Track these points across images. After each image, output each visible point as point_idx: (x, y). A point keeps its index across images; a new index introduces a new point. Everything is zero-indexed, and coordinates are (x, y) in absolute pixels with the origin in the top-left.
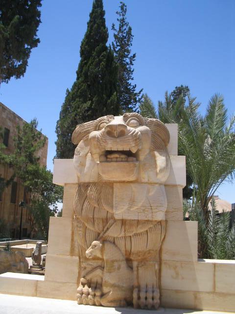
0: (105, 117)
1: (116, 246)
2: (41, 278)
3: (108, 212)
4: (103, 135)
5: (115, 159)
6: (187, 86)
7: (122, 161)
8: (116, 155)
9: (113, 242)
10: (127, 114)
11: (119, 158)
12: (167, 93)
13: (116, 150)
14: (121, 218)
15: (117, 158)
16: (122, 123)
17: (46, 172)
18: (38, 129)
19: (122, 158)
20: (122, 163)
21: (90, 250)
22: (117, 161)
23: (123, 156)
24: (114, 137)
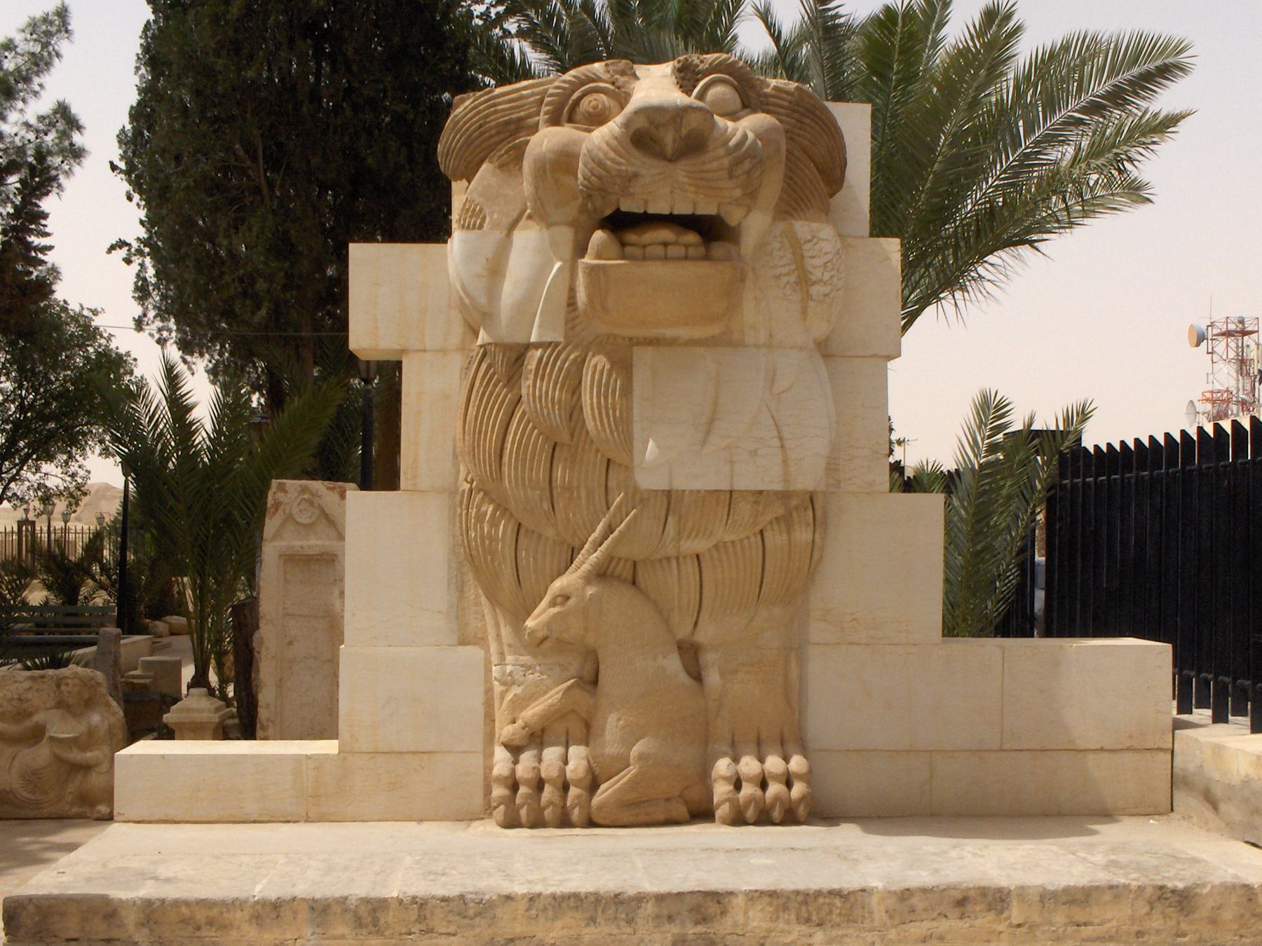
0: (598, 67)
1: (645, 594)
2: (327, 747)
3: (609, 460)
4: (617, 144)
5: (659, 250)
6: (71, 177)
7: (686, 258)
8: (665, 234)
9: (630, 577)
10: (695, 58)
11: (675, 243)
12: (114, 167)
13: (666, 212)
14: (663, 485)
15: (665, 244)
16: (678, 98)
17: (51, 288)
18: (121, 152)
19: (687, 246)
20: (688, 264)
21: (544, 617)
22: (666, 258)
23: (692, 238)
24: (661, 155)
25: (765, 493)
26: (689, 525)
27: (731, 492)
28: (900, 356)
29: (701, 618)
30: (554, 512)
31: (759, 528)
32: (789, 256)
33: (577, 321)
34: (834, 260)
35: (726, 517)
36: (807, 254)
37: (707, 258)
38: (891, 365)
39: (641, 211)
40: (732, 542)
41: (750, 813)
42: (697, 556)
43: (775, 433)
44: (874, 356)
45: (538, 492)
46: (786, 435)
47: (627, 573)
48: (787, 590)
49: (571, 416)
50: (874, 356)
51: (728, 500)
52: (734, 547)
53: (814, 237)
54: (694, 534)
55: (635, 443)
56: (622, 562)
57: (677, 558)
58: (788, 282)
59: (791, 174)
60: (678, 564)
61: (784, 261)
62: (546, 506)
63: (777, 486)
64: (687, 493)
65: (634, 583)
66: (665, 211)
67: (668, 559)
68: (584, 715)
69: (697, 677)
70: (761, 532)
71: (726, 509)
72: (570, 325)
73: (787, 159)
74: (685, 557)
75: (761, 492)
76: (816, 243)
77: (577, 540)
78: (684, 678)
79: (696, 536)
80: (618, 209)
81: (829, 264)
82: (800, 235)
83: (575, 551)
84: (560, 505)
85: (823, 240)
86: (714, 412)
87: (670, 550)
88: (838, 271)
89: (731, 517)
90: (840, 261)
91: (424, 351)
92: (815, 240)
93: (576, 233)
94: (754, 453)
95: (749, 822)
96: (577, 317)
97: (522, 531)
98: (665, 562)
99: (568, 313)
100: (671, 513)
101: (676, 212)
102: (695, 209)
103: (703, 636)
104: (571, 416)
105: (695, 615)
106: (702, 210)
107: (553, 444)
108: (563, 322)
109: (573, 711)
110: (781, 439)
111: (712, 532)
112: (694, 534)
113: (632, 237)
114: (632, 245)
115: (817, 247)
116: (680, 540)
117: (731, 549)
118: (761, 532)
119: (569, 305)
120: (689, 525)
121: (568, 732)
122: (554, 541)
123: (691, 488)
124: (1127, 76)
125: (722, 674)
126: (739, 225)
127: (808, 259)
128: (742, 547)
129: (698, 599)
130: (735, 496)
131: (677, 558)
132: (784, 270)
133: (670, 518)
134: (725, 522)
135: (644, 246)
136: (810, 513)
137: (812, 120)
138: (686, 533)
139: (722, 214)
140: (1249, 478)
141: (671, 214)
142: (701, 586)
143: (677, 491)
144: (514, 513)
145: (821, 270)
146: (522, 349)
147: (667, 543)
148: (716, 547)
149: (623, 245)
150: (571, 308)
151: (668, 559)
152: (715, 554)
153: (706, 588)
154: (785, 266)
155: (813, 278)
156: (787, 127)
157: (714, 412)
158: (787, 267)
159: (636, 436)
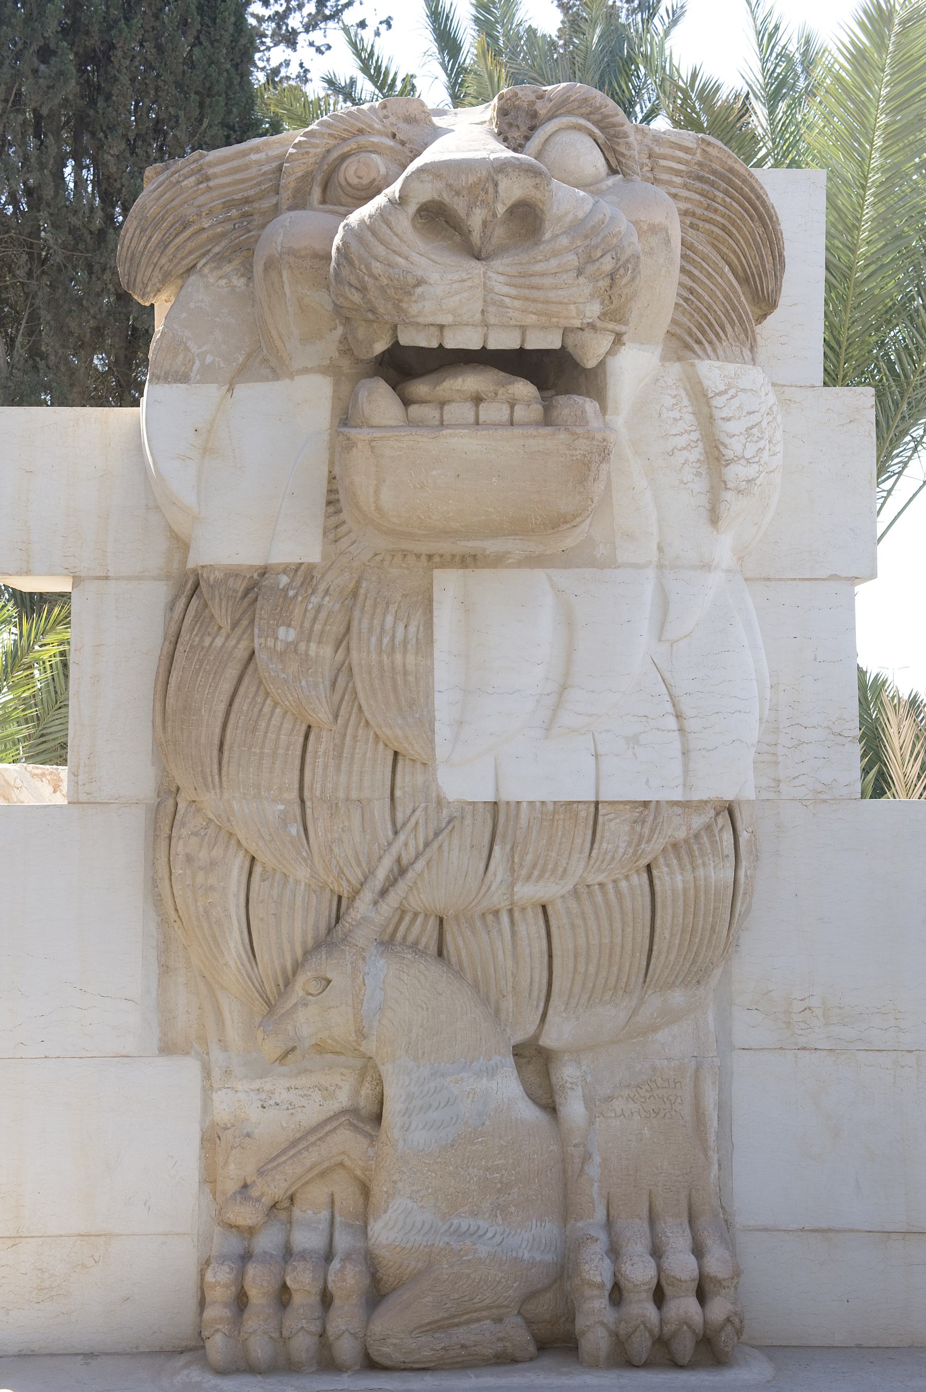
3: (396, 754)
15: (478, 400)
23: (523, 389)
25: (653, 805)
26: (529, 858)
27: (597, 803)
28: (873, 575)
29: (550, 1012)
30: (308, 843)
31: (644, 862)
32: (689, 418)
33: (343, 529)
34: (764, 424)
35: (588, 845)
36: (718, 414)
37: (547, 420)
38: (861, 589)
39: (516, 346)
40: (601, 885)
41: (685, 1347)
42: (544, 907)
43: (669, 707)
44: (834, 577)
45: (281, 807)
46: (687, 711)
47: (429, 939)
48: (694, 962)
49: (334, 684)
50: (834, 577)
51: (591, 818)
52: (605, 893)
53: (729, 386)
54: (536, 873)
55: (437, 725)
56: (420, 919)
57: (511, 911)
58: (686, 461)
59: (690, 283)
60: (512, 922)
61: (681, 426)
62: (295, 829)
63: (677, 795)
64: (524, 805)
65: (440, 953)
66: (474, 344)
67: (496, 913)
68: (358, 1173)
69: (551, 1109)
70: (649, 868)
71: (590, 832)
72: (331, 536)
73: (684, 257)
74: (523, 910)
75: (646, 804)
76: (733, 397)
77: (345, 884)
78: (528, 1112)
79: (540, 877)
80: (396, 344)
81: (755, 431)
82: (706, 383)
83: (344, 902)
84: (318, 830)
85: (744, 390)
86: (567, 674)
87: (498, 899)
88: (770, 442)
89: (596, 846)
90: (774, 425)
91: (107, 578)
92: (732, 392)
93: (336, 385)
94: (634, 740)
95: (681, 1362)
96: (344, 522)
97: (258, 869)
98: (490, 918)
99: (328, 516)
100: (498, 840)
101: (491, 346)
102: (523, 341)
103: (549, 1040)
104: (334, 684)
105: (542, 1004)
106: (536, 342)
107: (304, 728)
108: (321, 531)
109: (341, 1164)
110: (679, 716)
111: (565, 870)
112: (536, 873)
113: (420, 388)
114: (422, 402)
115: (736, 402)
116: (512, 885)
117: (599, 898)
118: (649, 868)
119: (329, 503)
120: (529, 858)
121: (333, 1202)
122: (308, 885)
123: (537, 797)
124: (730, 151)
125: (589, 1101)
126: (602, 364)
127: (720, 422)
128: (618, 892)
129: (545, 981)
130: (602, 810)
131: (511, 911)
132: (682, 441)
133: (497, 848)
134: (587, 854)
135: (442, 404)
136: (728, 836)
137: (726, 193)
138: (524, 872)
139: (570, 349)
140: (369, 652)
141: (521, 349)
142: (550, 956)
143: (508, 803)
144: (243, 842)
145: (742, 439)
146: (256, 576)
147: (493, 888)
148: (575, 892)
149: (407, 402)
150: (331, 509)
151: (496, 913)
152: (573, 905)
153: (557, 962)
154: (681, 434)
155: (729, 454)
156: (684, 206)
157: (567, 674)
158: (685, 436)
159: (438, 715)
